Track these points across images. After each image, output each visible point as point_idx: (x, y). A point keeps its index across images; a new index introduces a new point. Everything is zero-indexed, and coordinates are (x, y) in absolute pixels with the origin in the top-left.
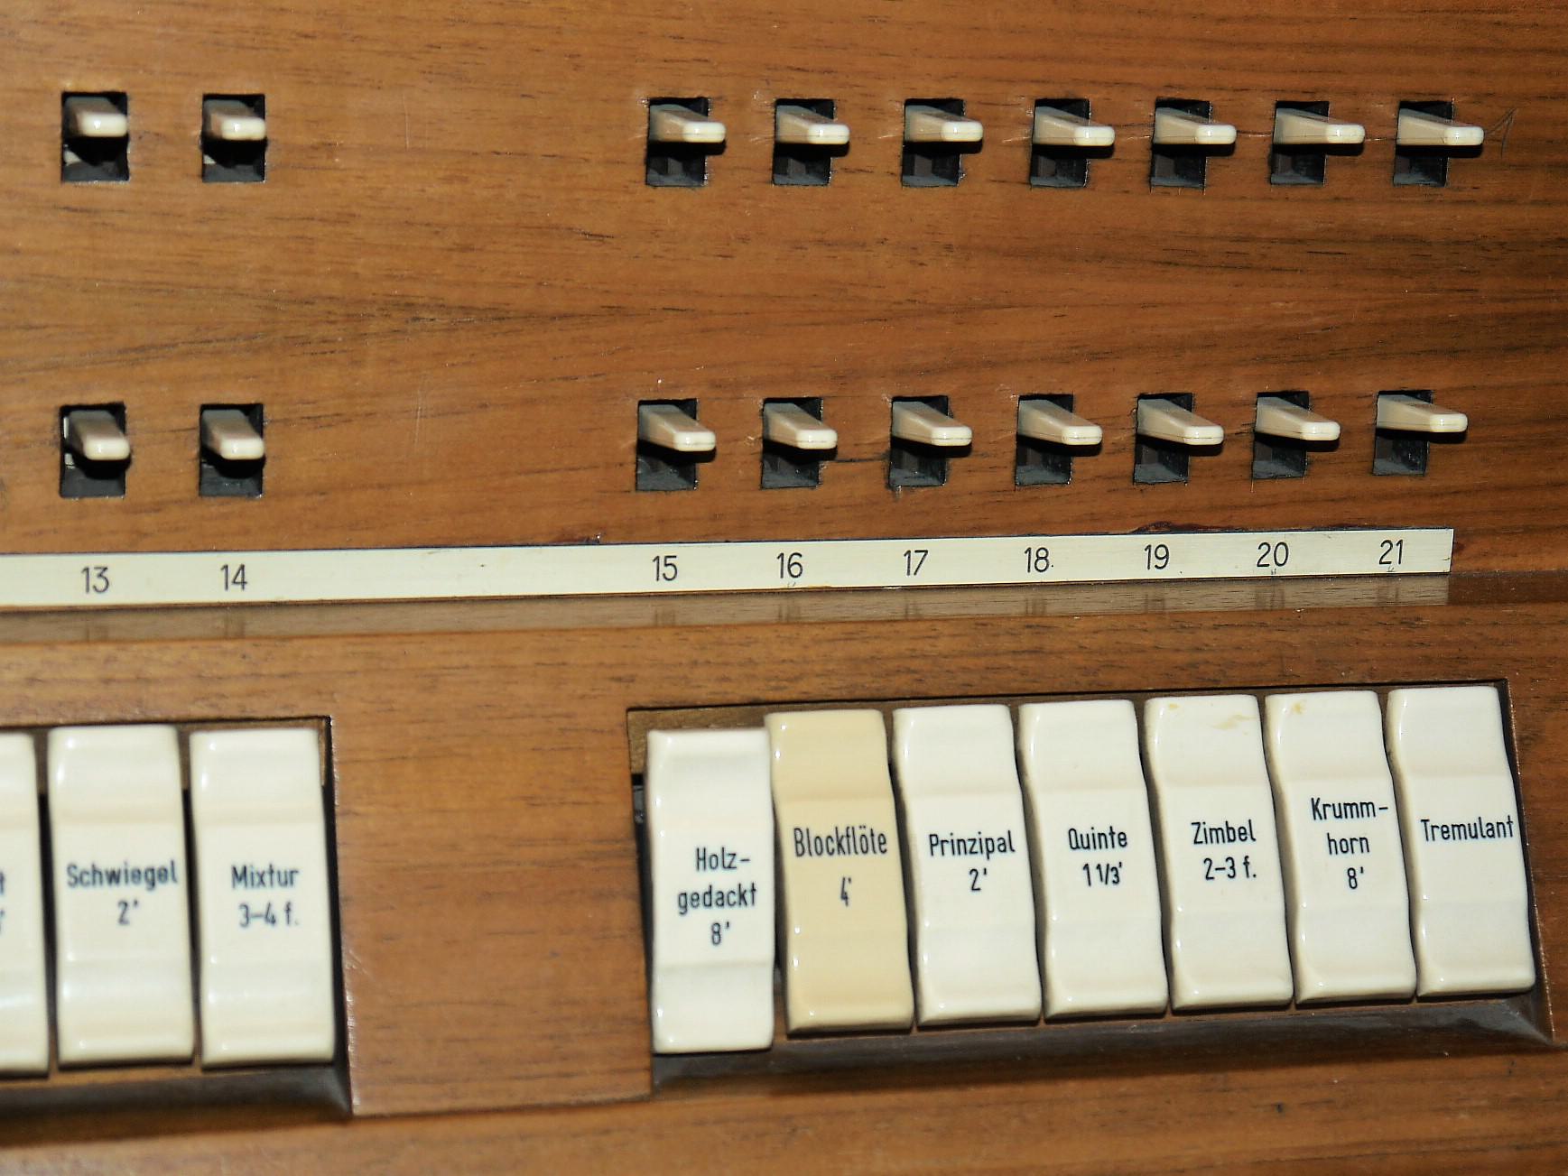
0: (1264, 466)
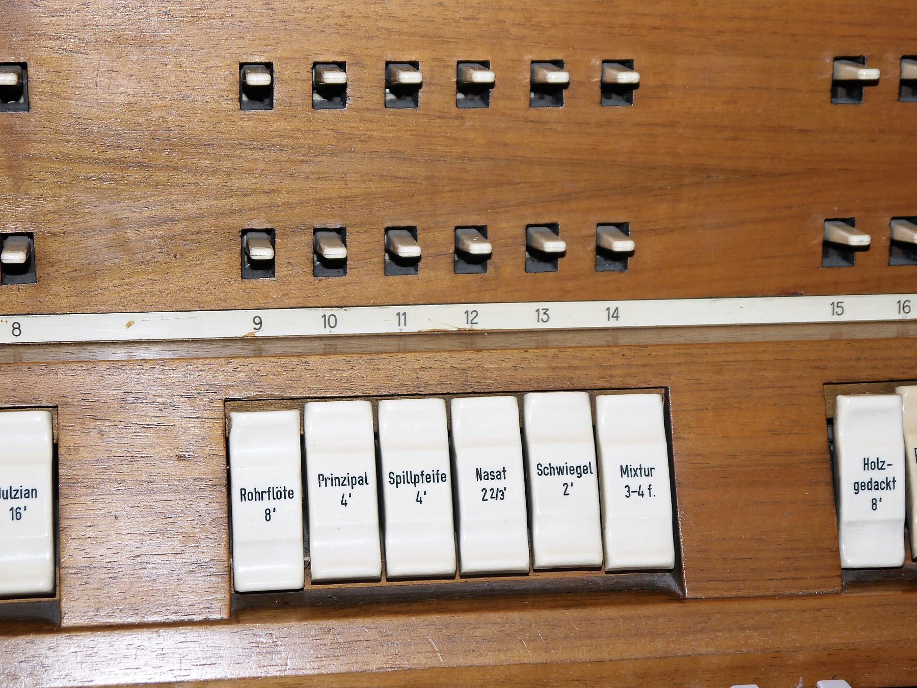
0: (899, 260)
